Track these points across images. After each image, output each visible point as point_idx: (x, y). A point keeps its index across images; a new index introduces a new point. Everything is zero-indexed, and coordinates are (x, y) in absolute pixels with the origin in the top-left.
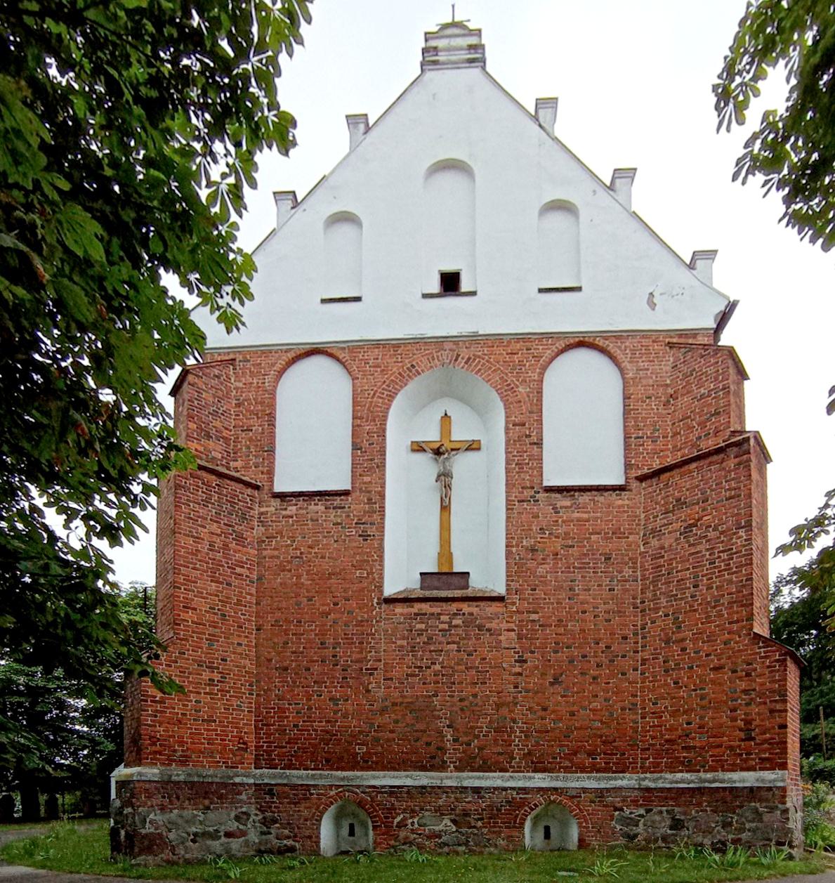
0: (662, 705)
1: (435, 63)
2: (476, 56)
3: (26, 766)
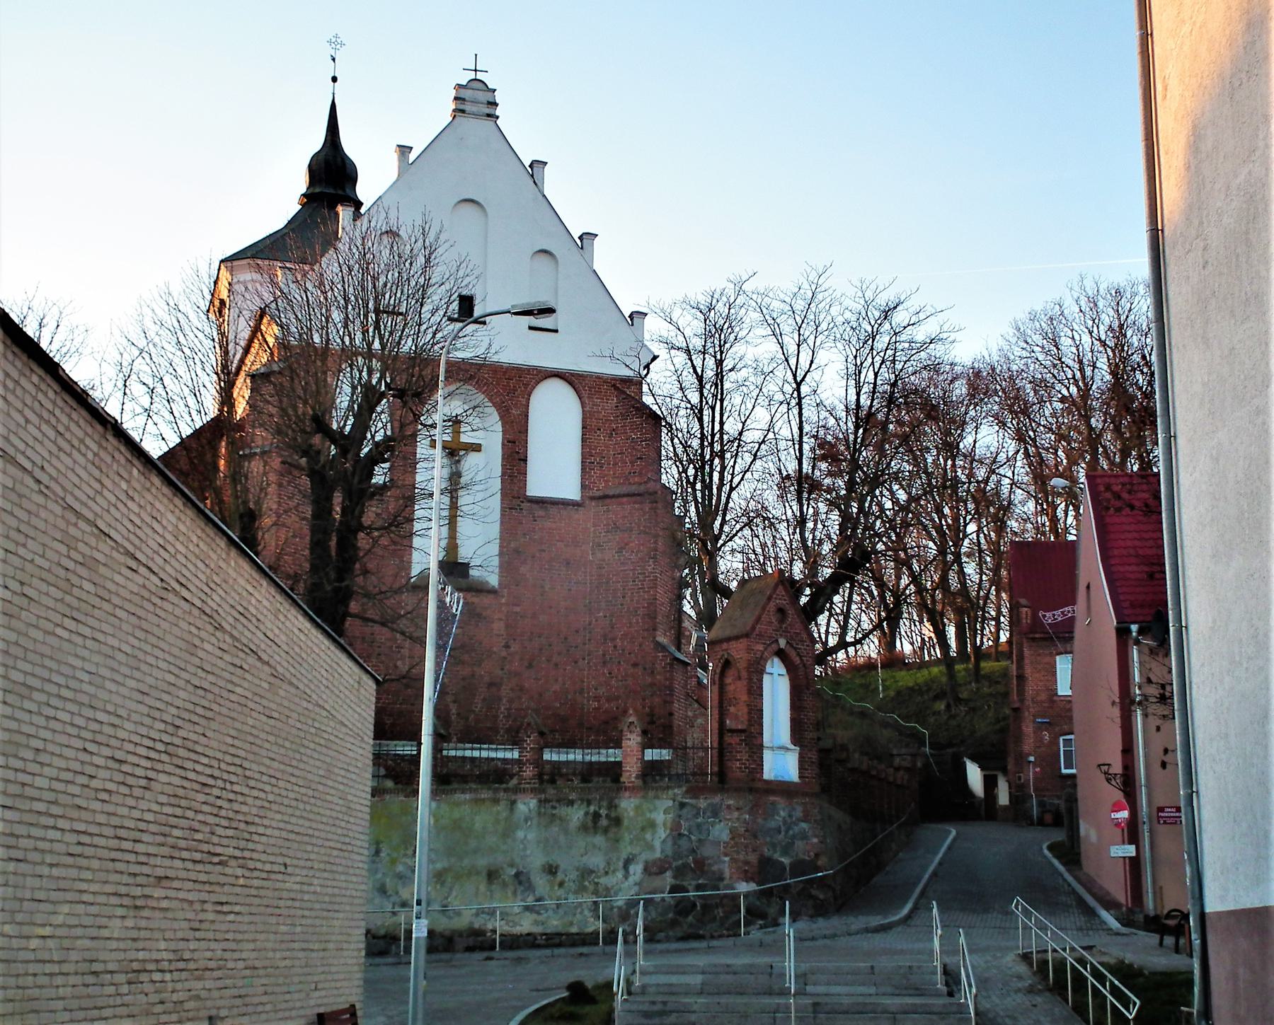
0: (601, 691)
1: (463, 111)
2: (490, 110)
3: (356, 538)
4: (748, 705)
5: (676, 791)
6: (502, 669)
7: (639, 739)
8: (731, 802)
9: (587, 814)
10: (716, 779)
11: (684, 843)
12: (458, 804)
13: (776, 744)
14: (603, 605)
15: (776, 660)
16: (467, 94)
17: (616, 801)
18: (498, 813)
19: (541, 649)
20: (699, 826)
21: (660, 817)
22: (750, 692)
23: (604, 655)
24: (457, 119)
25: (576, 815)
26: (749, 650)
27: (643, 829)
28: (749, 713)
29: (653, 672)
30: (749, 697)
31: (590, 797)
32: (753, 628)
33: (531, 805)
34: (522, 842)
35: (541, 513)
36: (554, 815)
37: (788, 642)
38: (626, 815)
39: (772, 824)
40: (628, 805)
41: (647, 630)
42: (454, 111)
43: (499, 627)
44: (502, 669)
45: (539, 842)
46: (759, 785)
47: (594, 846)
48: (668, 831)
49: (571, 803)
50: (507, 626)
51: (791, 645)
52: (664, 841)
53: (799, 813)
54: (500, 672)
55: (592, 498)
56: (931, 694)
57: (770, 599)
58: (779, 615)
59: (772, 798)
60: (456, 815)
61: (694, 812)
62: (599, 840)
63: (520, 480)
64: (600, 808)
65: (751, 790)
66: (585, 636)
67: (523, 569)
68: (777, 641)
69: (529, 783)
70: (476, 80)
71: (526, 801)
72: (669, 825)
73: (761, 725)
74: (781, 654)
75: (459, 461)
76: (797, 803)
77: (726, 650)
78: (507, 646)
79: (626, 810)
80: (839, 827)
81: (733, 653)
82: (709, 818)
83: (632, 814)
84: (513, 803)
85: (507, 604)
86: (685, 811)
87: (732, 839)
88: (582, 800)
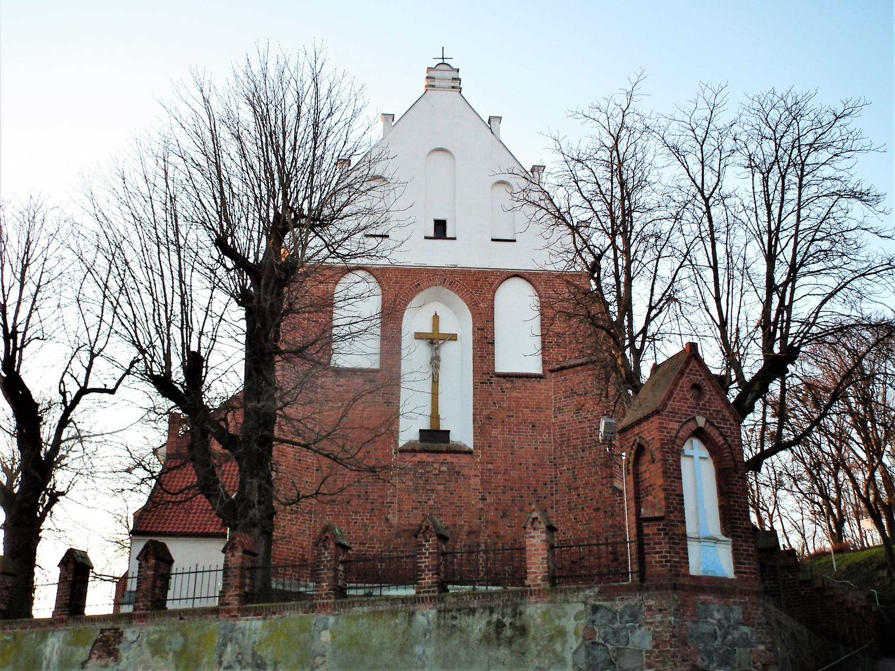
2: (456, 85)
4: (665, 490)
5: (587, 592)
6: (480, 519)
7: (544, 536)
8: (652, 603)
9: (489, 623)
10: (637, 579)
11: (599, 653)
12: (356, 618)
13: (703, 534)
14: (566, 460)
15: (696, 442)
16: (432, 74)
17: (522, 608)
18: (396, 626)
19: (513, 500)
20: (616, 632)
21: (570, 624)
22: (665, 474)
23: (569, 503)
24: (429, 92)
25: (478, 625)
26: (661, 429)
27: (551, 639)
28: (666, 498)
29: (613, 515)
30: (666, 481)
31: (493, 605)
32: (664, 405)
33: (430, 616)
34: (420, 658)
35: (509, 385)
36: (454, 626)
37: (707, 420)
38: (532, 623)
39: (706, 628)
40: (534, 610)
41: (605, 478)
42: (426, 86)
43: (475, 482)
44: (480, 519)
45: (438, 658)
46: (682, 581)
47: (497, 660)
48: (580, 640)
49: (472, 611)
50: (482, 481)
51: (712, 424)
52: (575, 652)
53: (737, 614)
54: (478, 521)
55: (552, 371)
56: (875, 566)
57: (682, 373)
58: (695, 393)
59: (702, 597)
60: (354, 630)
61: (610, 616)
62: (503, 652)
63: (488, 360)
64: (503, 618)
65: (675, 588)
66: (552, 488)
67: (494, 432)
68: (694, 418)
69: (428, 592)
70: (443, 63)
71: (425, 612)
72: (581, 632)
73: (682, 511)
74: (699, 433)
75: (437, 348)
76: (735, 603)
77: (638, 434)
78: (483, 499)
79: (532, 617)
80: (793, 636)
81: (647, 436)
82: (627, 622)
83: (539, 621)
84: (412, 614)
85: (482, 463)
86: (599, 615)
87: (657, 646)
88: (484, 608)
